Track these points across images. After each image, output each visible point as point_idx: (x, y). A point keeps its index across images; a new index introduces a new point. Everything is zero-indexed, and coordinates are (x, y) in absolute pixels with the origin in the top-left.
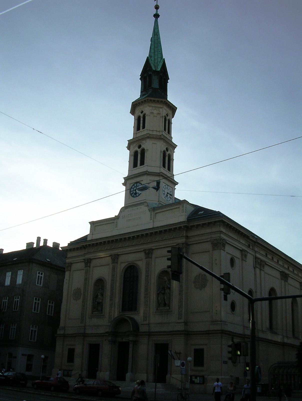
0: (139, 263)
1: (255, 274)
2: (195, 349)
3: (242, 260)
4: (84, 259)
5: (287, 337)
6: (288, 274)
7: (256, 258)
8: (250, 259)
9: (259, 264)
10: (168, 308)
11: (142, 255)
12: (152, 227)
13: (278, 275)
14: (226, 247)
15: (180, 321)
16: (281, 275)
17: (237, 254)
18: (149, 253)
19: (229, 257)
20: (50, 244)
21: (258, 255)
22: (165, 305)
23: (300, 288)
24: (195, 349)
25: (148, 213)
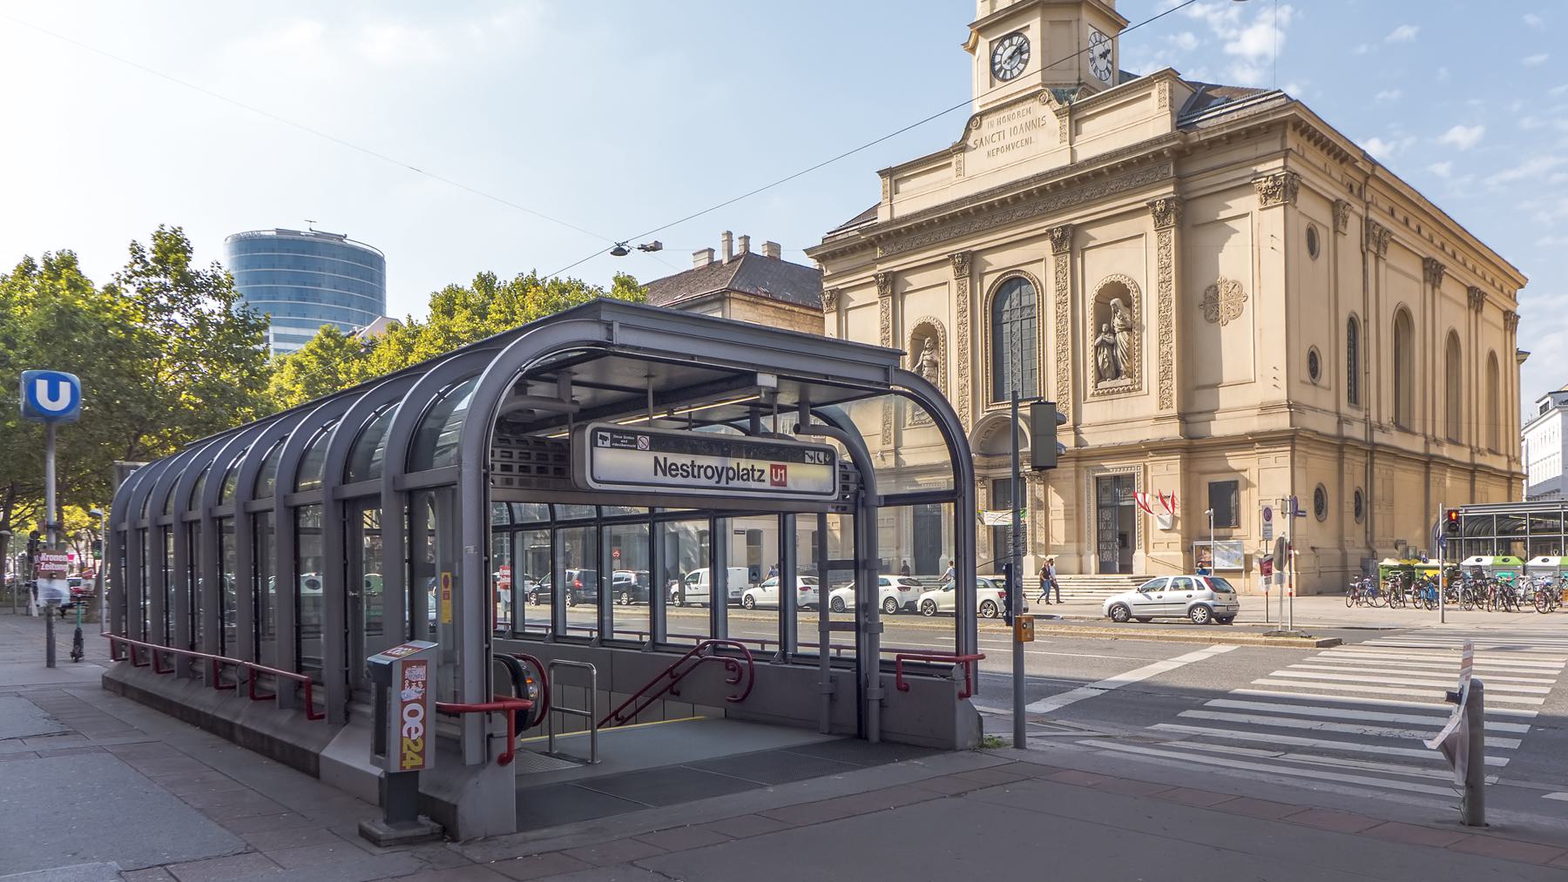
0: (1034, 270)
1: (1365, 271)
2: (1210, 484)
3: (1336, 231)
4: (876, 276)
5: (1381, 427)
6: (1442, 267)
7: (1368, 223)
8: (1354, 226)
9: (1375, 240)
10: (1128, 381)
11: (1045, 247)
12: (1066, 162)
13: (1417, 270)
14: (1299, 196)
15: (1165, 412)
16: (1425, 269)
17: (1323, 216)
18: (1069, 242)
19: (1304, 225)
20: (757, 248)
21: (1372, 215)
22: (1117, 374)
23: (1465, 303)
24: (1210, 484)
25: (1053, 123)
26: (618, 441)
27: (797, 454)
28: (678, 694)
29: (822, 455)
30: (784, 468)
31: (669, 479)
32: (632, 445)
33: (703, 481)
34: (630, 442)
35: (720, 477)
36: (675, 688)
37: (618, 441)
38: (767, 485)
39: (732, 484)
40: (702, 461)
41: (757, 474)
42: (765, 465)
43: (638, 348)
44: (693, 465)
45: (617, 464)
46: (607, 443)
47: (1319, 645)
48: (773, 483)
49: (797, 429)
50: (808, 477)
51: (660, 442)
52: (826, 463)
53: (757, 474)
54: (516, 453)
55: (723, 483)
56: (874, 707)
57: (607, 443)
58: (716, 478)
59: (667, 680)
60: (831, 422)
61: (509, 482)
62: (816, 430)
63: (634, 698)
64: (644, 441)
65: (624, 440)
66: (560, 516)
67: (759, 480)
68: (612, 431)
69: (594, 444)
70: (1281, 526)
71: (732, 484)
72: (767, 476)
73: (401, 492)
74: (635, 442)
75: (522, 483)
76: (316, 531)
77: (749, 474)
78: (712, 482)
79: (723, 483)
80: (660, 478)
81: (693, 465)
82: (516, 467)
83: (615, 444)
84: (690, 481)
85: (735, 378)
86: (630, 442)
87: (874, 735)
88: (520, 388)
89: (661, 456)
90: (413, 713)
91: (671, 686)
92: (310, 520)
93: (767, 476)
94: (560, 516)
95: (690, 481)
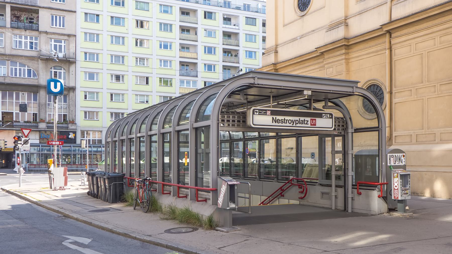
26: (261, 113)
27: (320, 116)
28: (283, 196)
29: (328, 115)
30: (315, 120)
31: (277, 124)
32: (265, 114)
33: (288, 124)
34: (264, 113)
35: (293, 123)
36: (282, 194)
37: (261, 113)
38: (309, 125)
39: (297, 125)
40: (287, 118)
41: (306, 122)
42: (309, 119)
43: (263, 85)
44: (285, 120)
45: (261, 120)
46: (258, 113)
47: (90, 211)
48: (311, 125)
49: (324, 107)
50: (325, 123)
51: (273, 113)
52: (330, 118)
53: (306, 122)
54: (236, 116)
55: (294, 125)
56: (350, 200)
57: (258, 113)
58: (292, 123)
59: (280, 191)
60: (337, 105)
61: (229, 125)
62: (330, 107)
63: (269, 197)
64: (269, 113)
65: (263, 112)
66: (153, 144)
67: (306, 124)
68: (259, 110)
69: (253, 114)
70: (58, 171)
71: (297, 125)
72: (309, 123)
73: (194, 128)
74: (266, 113)
75: (238, 125)
76: (156, 142)
77: (303, 122)
78: (291, 125)
79: (294, 125)
80: (274, 124)
81: (285, 120)
82: (236, 121)
83: (260, 113)
84: (284, 124)
85: (296, 92)
86: (264, 113)
87: (350, 210)
88: (230, 96)
89: (274, 117)
90: (396, 186)
91: (281, 193)
92: (154, 138)
93: (309, 123)
94: (153, 144)
95: (284, 124)
